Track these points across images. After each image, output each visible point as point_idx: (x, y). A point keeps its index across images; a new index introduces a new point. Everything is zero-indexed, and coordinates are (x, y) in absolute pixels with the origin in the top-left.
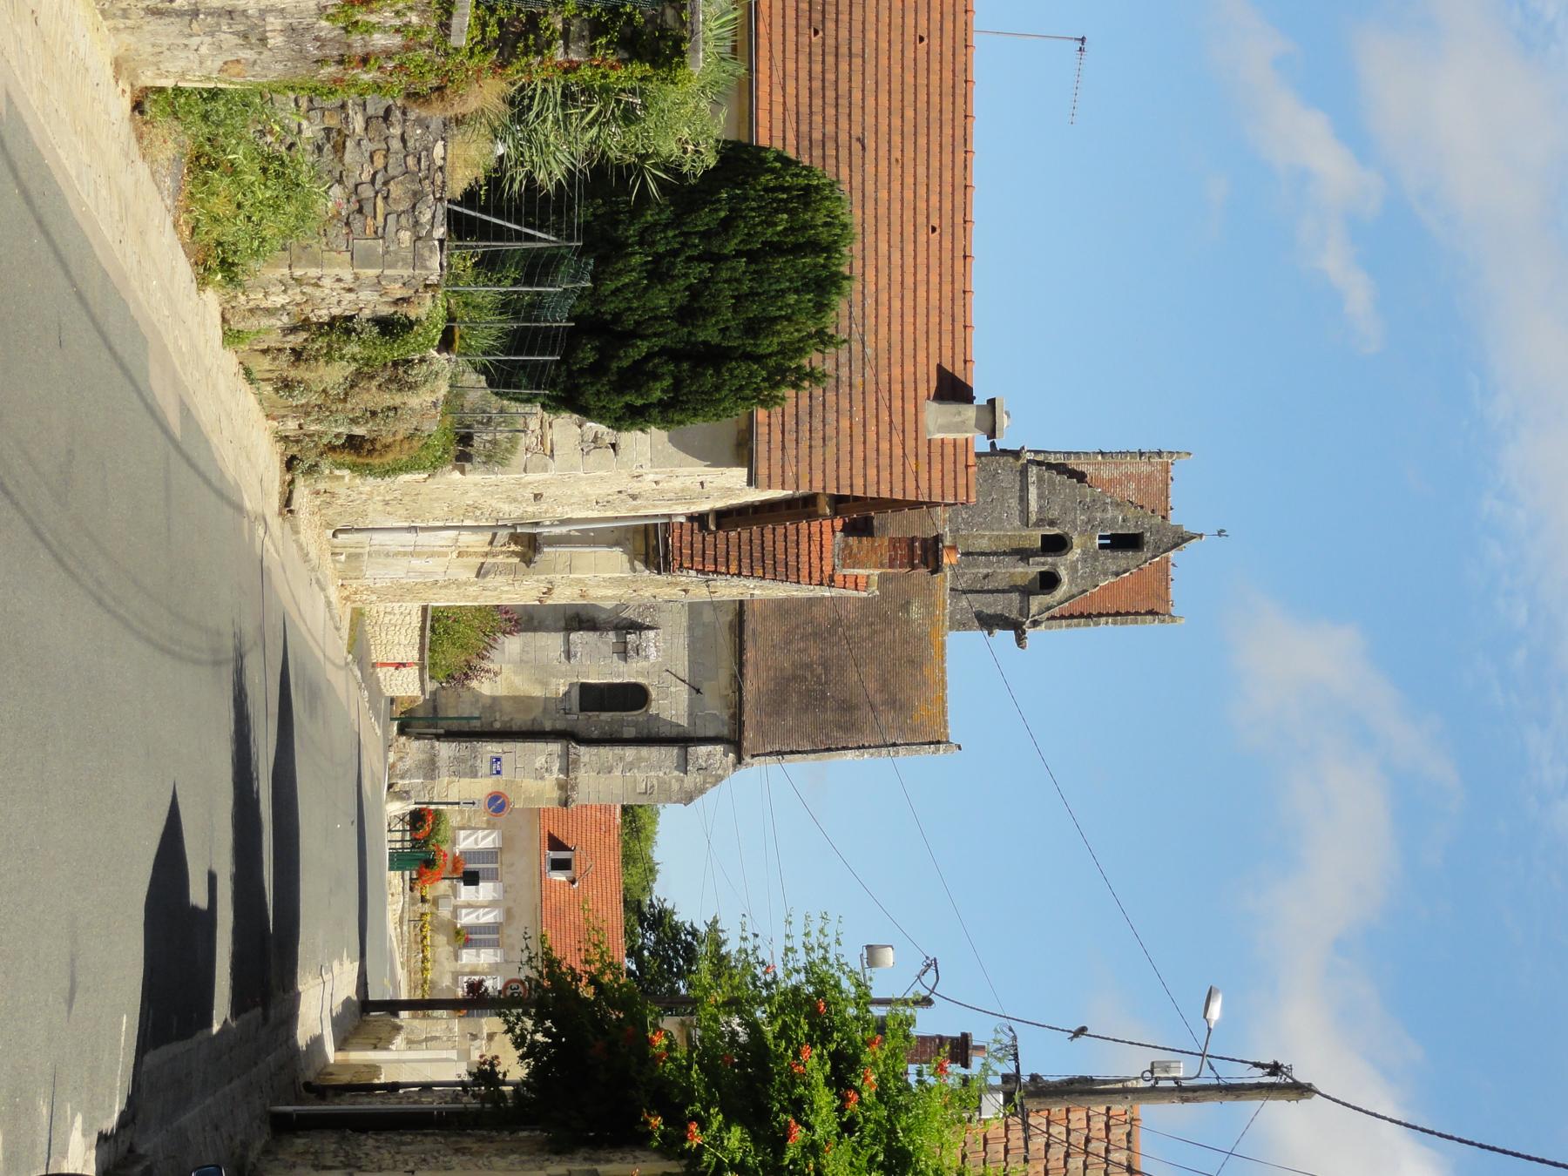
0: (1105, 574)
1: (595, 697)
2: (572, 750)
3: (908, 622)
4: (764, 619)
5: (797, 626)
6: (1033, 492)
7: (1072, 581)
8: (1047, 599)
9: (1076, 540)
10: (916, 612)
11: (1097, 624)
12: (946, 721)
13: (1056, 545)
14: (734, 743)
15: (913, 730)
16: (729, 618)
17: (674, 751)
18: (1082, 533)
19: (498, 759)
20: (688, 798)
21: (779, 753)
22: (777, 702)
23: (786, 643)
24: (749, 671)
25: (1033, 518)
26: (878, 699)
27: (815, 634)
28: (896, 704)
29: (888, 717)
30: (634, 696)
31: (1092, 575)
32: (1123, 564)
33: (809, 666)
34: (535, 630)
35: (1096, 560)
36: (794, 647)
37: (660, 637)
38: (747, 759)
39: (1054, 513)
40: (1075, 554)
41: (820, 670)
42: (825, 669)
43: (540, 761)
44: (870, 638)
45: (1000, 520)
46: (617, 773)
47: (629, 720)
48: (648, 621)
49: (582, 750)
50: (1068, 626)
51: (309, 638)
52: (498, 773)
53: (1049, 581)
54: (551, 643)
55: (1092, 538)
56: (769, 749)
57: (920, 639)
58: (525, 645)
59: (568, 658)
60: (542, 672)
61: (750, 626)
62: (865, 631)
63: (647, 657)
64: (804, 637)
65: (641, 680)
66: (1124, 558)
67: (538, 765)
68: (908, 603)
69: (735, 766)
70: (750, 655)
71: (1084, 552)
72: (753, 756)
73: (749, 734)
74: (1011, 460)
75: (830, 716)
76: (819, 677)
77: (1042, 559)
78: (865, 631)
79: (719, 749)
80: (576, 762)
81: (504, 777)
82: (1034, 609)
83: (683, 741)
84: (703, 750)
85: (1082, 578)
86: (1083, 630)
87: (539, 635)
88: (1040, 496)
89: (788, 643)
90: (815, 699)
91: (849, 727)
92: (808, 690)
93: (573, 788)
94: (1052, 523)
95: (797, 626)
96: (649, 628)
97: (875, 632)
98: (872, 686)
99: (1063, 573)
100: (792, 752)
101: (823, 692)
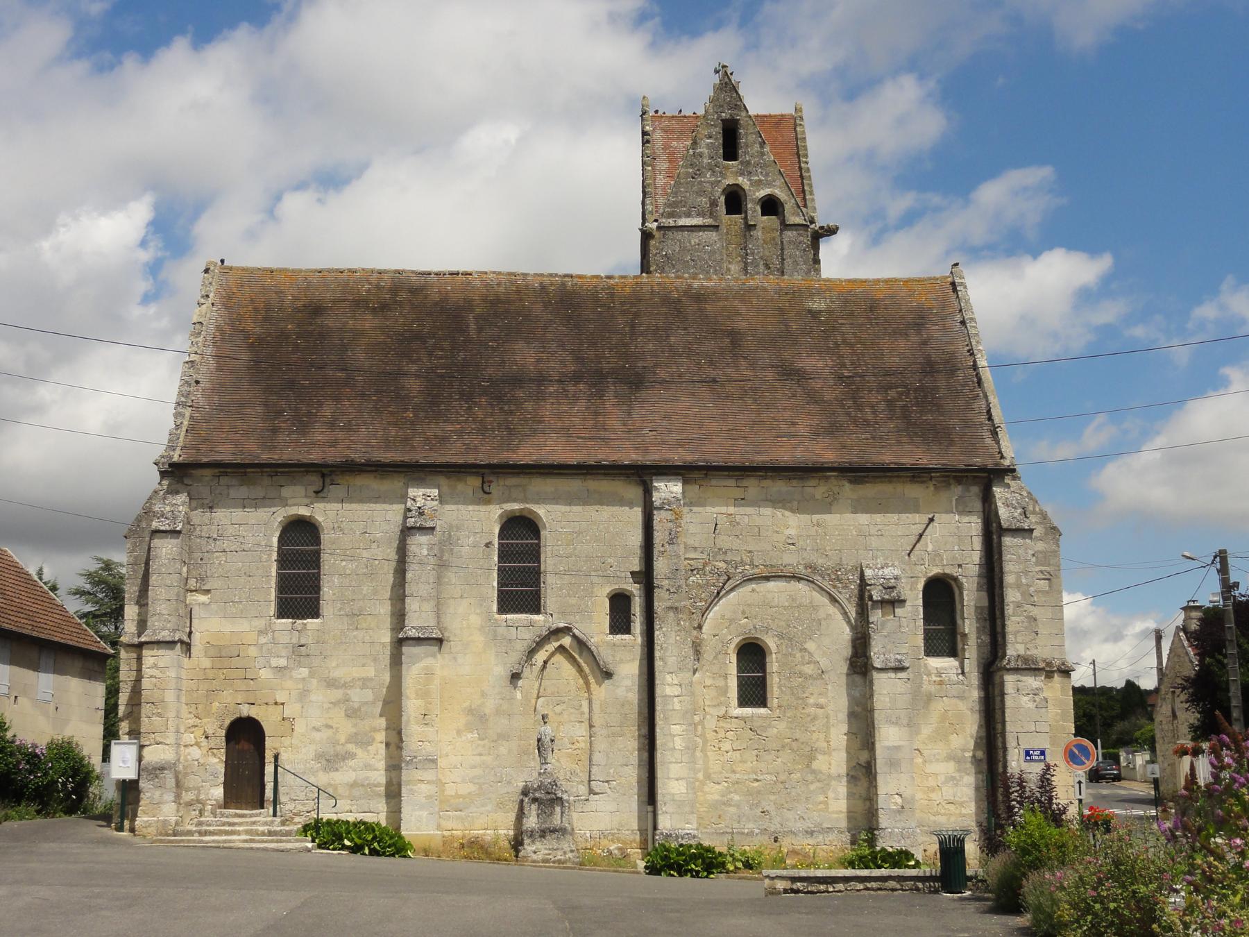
0: (763, 154)
1: (942, 637)
2: (1013, 665)
3: (830, 312)
4: (844, 447)
5: (848, 414)
6: (683, 221)
7: (769, 184)
8: (789, 207)
9: (730, 181)
10: (818, 305)
11: (808, 170)
12: (930, 279)
13: (735, 201)
14: (988, 477)
15: (944, 307)
16: (847, 486)
17: (1007, 541)
18: (724, 176)
19: (1027, 753)
20: (1054, 531)
21: (994, 433)
22: (938, 435)
23: (868, 425)
24: (908, 460)
25: (708, 221)
26: (915, 338)
27: (854, 398)
28: (919, 321)
29: (934, 329)
30: (940, 594)
31: (764, 166)
32: (752, 138)
33: (890, 404)
34: (872, 711)
35: (748, 163)
36: (870, 417)
37: (871, 563)
38: (1006, 463)
39: (704, 200)
40: (743, 181)
41: (892, 394)
42: (891, 388)
43: (1026, 702)
44: (852, 346)
45: (712, 253)
46: (1035, 612)
47: (970, 598)
48: (857, 575)
49: (1011, 651)
50: (811, 193)
51: (238, 811)
52: (1043, 753)
53: (771, 206)
54: (886, 687)
55: (727, 168)
56: (989, 441)
57: (846, 301)
58: (890, 722)
59: (903, 669)
60: (921, 701)
61: (852, 457)
62: (845, 350)
63: (896, 578)
64: (859, 408)
65: (921, 586)
66: (747, 138)
67: (1031, 705)
68: (810, 311)
69: (1015, 478)
70: (888, 458)
71: (742, 174)
72: (1002, 457)
73: (978, 461)
74: (652, 242)
75: (942, 383)
76: (901, 394)
77: (750, 212)
78: (845, 350)
79: (998, 491)
80: (1026, 660)
81: (1046, 745)
82: (798, 220)
83: (993, 534)
84: (1003, 512)
85: (767, 175)
86: (814, 181)
87: (877, 705)
88: (688, 215)
89: (867, 423)
90: (926, 398)
91: (950, 366)
92: (917, 404)
93: (1049, 664)
94: (714, 204)
95: (848, 414)
96: (862, 573)
97: (844, 341)
98: (902, 343)
99: (762, 193)
100: (990, 418)
101: (916, 390)
